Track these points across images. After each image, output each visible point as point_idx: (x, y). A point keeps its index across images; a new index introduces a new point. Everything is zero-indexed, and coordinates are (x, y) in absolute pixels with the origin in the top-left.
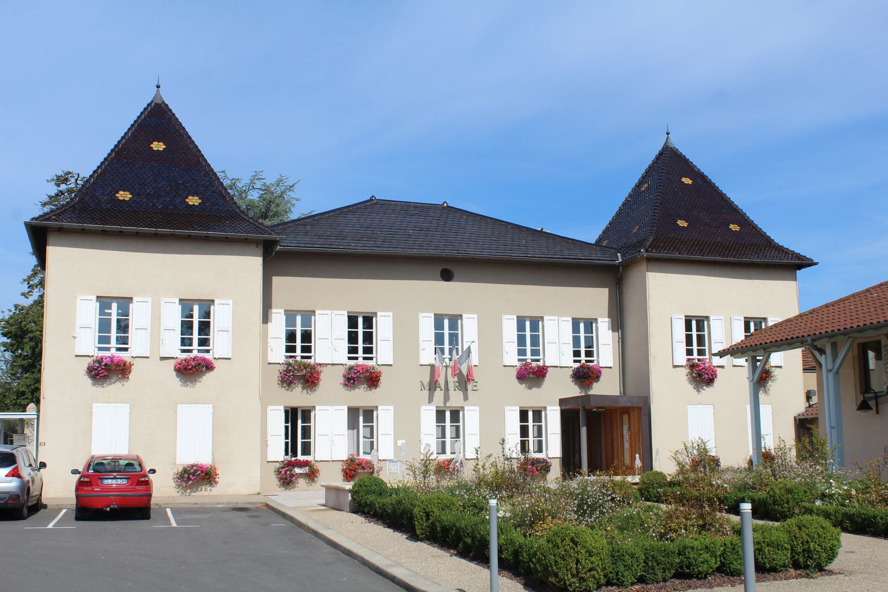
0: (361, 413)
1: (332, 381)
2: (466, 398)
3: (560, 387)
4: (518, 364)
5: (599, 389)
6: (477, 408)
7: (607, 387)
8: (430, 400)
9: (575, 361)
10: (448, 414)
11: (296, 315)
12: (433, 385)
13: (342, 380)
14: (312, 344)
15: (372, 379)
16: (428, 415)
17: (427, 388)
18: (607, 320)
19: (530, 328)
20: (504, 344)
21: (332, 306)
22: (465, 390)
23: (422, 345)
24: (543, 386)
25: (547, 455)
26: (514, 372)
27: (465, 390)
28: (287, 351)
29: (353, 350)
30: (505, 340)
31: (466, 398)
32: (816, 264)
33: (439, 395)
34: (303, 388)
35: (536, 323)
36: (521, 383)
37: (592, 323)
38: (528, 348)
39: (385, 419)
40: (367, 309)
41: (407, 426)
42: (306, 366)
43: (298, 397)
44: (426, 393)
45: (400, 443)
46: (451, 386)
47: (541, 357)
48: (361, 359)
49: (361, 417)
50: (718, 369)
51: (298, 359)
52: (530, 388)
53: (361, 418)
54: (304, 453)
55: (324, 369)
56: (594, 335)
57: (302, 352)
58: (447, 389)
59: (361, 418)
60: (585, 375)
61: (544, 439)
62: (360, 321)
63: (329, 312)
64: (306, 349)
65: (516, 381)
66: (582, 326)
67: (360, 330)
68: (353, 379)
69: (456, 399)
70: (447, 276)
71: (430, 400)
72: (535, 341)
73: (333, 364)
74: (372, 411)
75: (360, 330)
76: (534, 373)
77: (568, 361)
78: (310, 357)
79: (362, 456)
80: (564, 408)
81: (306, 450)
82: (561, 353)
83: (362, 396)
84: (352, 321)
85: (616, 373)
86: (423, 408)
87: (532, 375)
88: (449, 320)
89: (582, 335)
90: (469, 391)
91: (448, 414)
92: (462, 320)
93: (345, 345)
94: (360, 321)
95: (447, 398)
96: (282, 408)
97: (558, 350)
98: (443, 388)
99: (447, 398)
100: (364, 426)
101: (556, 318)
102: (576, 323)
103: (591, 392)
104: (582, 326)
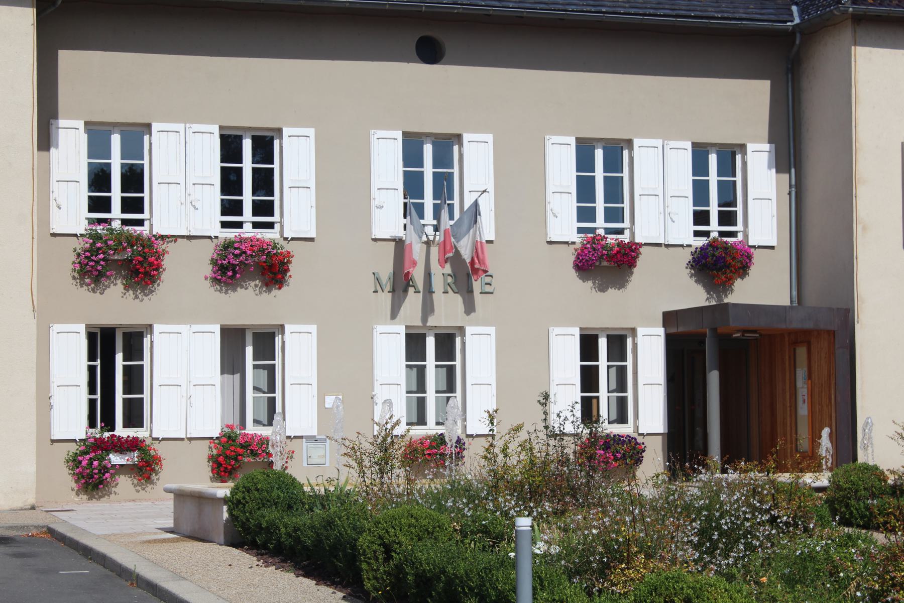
0: (249, 338)
1: (185, 273)
2: (470, 308)
5: (745, 292)
6: (492, 330)
7: (764, 287)
8: (394, 315)
9: (697, 234)
10: (430, 342)
11: (110, 133)
12: (401, 283)
13: (208, 270)
14: (146, 195)
15: (272, 269)
16: (390, 344)
17: (388, 288)
18: (767, 147)
19: (604, 162)
20: (550, 197)
21: (187, 116)
22: (466, 292)
23: (378, 197)
25: (636, 428)
26: (569, 257)
27: (466, 292)
28: (696, 222)
29: (231, 208)
30: (551, 187)
31: (470, 308)
34: (127, 287)
35: (616, 149)
36: (584, 278)
38: (116, 194)
39: (299, 351)
40: (262, 121)
41: (344, 368)
42: (134, 240)
43: (116, 305)
44: (386, 298)
46: (438, 283)
47: (626, 224)
48: (248, 227)
49: (248, 348)
51: (116, 225)
52: (602, 289)
53: (249, 351)
55: (170, 247)
56: (739, 179)
57: (720, 224)
58: (429, 290)
59: (249, 351)
60: (718, 263)
61: (630, 394)
62: (247, 145)
63: (180, 127)
64: (133, 205)
65: (573, 273)
66: (713, 159)
67: (247, 165)
68: (232, 267)
69: (448, 310)
70: (430, 52)
71: (394, 315)
72: (614, 190)
73: (190, 238)
74: (272, 336)
75: (247, 165)
76: (610, 258)
77: (683, 232)
78: (140, 223)
79: (251, 429)
80: (673, 330)
81: (134, 417)
82: (667, 216)
83: (250, 305)
84: (230, 147)
85: (783, 260)
86: (379, 328)
87: (607, 262)
88: (435, 145)
91: (430, 342)
92: (150, 135)
93: (214, 196)
94: (247, 145)
95: (428, 308)
97: (662, 210)
99: (428, 308)
100: (255, 367)
102: (700, 153)
104: (713, 159)
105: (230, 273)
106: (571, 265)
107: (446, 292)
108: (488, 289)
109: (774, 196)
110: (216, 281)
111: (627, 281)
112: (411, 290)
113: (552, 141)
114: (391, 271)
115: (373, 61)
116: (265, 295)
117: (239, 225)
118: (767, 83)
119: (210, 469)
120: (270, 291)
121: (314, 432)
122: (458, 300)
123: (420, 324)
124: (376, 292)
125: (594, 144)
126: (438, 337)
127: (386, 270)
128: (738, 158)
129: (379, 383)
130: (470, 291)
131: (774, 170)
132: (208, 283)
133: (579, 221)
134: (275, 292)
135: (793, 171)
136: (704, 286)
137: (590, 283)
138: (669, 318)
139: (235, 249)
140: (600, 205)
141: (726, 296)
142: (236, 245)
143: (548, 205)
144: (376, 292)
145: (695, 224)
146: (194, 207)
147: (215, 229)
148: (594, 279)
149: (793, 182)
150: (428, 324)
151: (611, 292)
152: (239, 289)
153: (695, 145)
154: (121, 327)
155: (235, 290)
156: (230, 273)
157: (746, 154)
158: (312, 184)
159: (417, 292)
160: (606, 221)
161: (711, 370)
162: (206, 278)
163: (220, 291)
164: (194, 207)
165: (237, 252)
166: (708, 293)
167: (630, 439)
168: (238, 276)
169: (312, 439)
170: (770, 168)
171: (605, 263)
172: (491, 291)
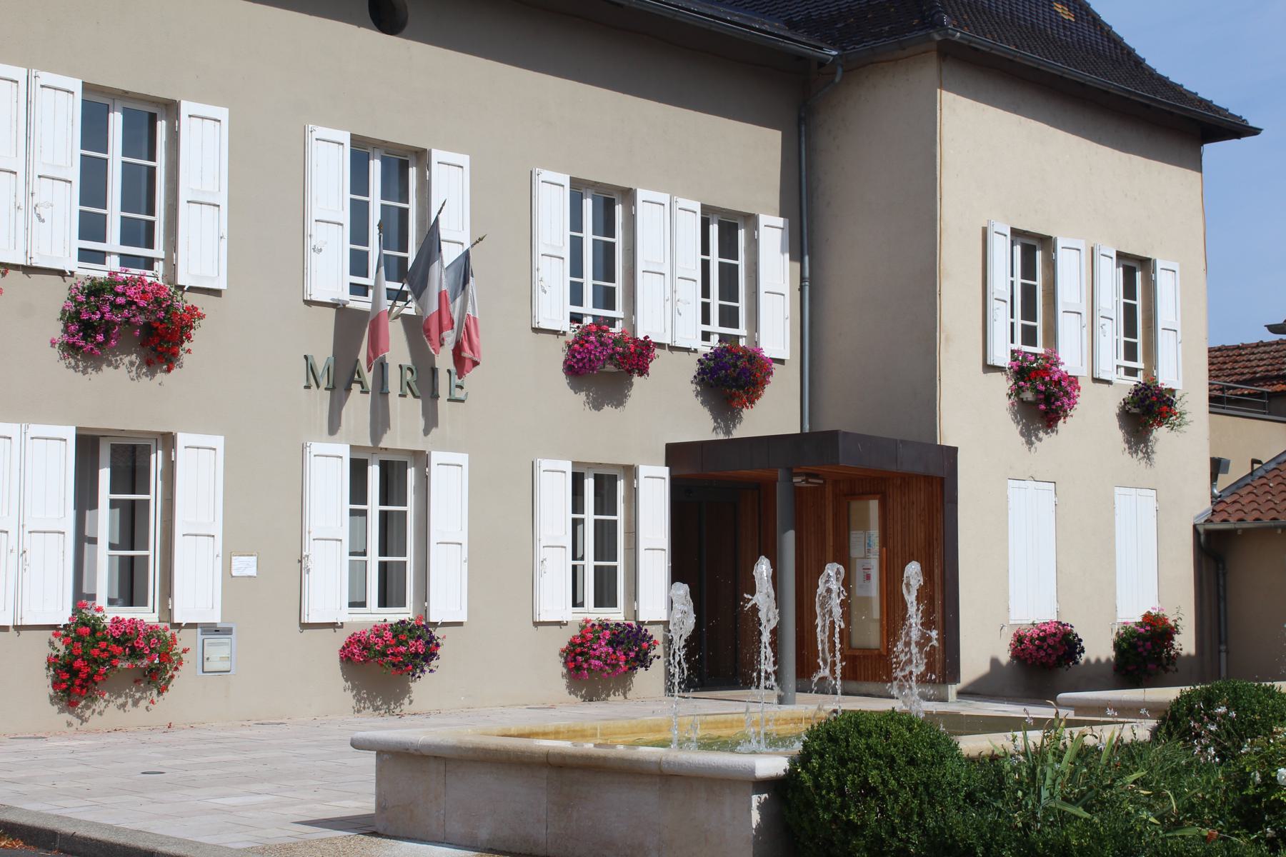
2: (431, 420)
3: (666, 409)
4: (565, 325)
8: (334, 426)
9: (85, 255)
11: (107, 110)
12: (342, 378)
13: (56, 330)
16: (327, 470)
17: (324, 383)
19: (605, 204)
23: (318, 234)
24: (629, 402)
25: (167, 612)
26: (557, 353)
30: (1160, 326)
31: (431, 420)
32: (1255, 131)
33: (358, 405)
36: (576, 387)
37: (153, 119)
39: (198, 481)
41: (265, 518)
44: (322, 398)
45: (245, 566)
47: (158, 251)
48: (113, 264)
50: (774, 365)
52: (597, 406)
53: (105, 475)
54: (599, 603)
56: (160, 164)
57: (124, 242)
60: (730, 376)
61: (153, 552)
65: (562, 379)
66: (116, 121)
68: (107, 327)
71: (334, 426)
72: (140, 189)
73: (29, 270)
78: (149, 263)
79: (110, 614)
80: (685, 471)
83: (121, 395)
87: (604, 361)
89: (115, 157)
90: (442, 403)
95: (380, 421)
96: (70, 433)
98: (369, 377)
99: (380, 421)
100: (113, 504)
101: (19, 73)
102: (95, 108)
103: (740, 432)
104: (116, 121)
105: (100, 338)
106: (560, 366)
107: (403, 395)
108: (458, 394)
109: (786, 289)
110: (70, 349)
111: (626, 396)
112: (356, 388)
113: (315, 135)
114: (330, 354)
115: (624, 92)
116: (145, 380)
117: (99, 257)
118: (775, 137)
119: (49, 681)
120: (153, 375)
121: (215, 617)
122: (414, 406)
123: (370, 444)
124: (308, 387)
125: (370, 150)
126: (598, 478)
127: (323, 354)
128: (161, 126)
129: (313, 536)
130: (435, 396)
131: (787, 256)
132: (56, 353)
133: (82, 237)
134: (160, 376)
135: (807, 259)
136: (711, 410)
137: (582, 396)
138: (676, 454)
139: (117, 294)
140: (114, 213)
141: (734, 426)
142: (120, 288)
143: (307, 240)
144: (308, 387)
145: (82, 236)
146: (39, 216)
147: (70, 262)
148: (588, 390)
149: (807, 274)
150: (382, 445)
151: (607, 409)
152: (104, 367)
153: (355, 140)
154: (107, 434)
155: (98, 369)
156: (100, 338)
157: (429, 167)
158: (223, 200)
159: (364, 392)
160: (123, 243)
161: (786, 531)
162: (53, 343)
163: (75, 368)
164: (39, 216)
165: (121, 300)
166: (716, 421)
167: (152, 631)
168: (113, 342)
169: (211, 629)
170: (783, 252)
171: (610, 368)
172: (462, 397)
